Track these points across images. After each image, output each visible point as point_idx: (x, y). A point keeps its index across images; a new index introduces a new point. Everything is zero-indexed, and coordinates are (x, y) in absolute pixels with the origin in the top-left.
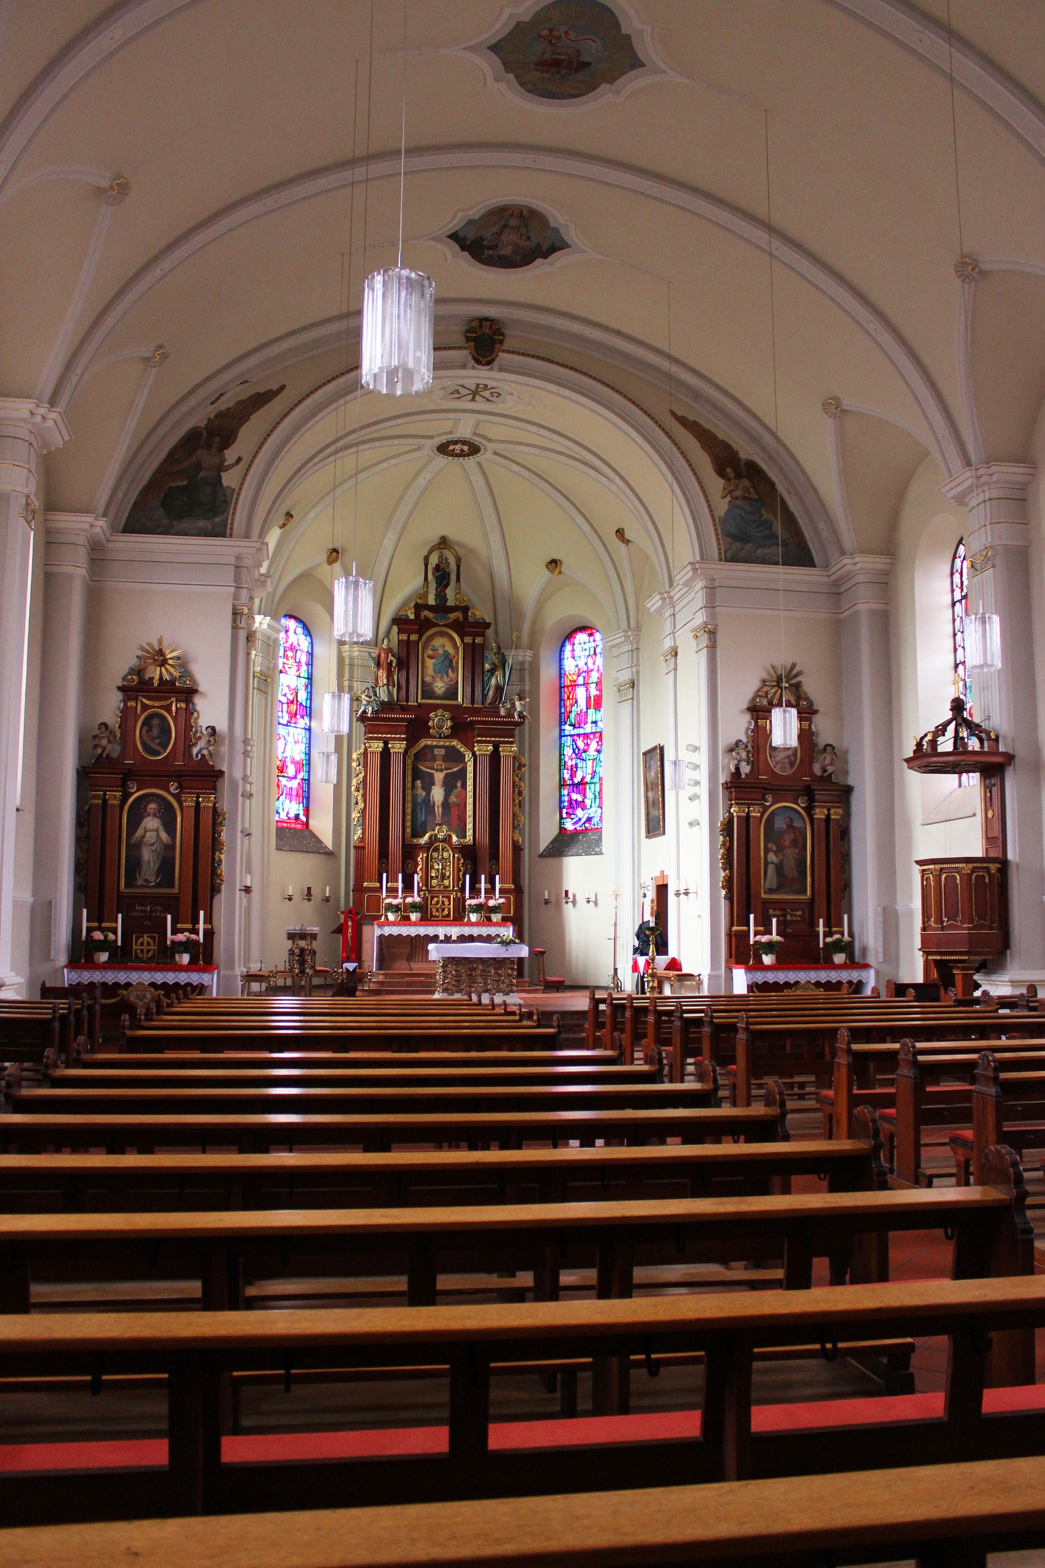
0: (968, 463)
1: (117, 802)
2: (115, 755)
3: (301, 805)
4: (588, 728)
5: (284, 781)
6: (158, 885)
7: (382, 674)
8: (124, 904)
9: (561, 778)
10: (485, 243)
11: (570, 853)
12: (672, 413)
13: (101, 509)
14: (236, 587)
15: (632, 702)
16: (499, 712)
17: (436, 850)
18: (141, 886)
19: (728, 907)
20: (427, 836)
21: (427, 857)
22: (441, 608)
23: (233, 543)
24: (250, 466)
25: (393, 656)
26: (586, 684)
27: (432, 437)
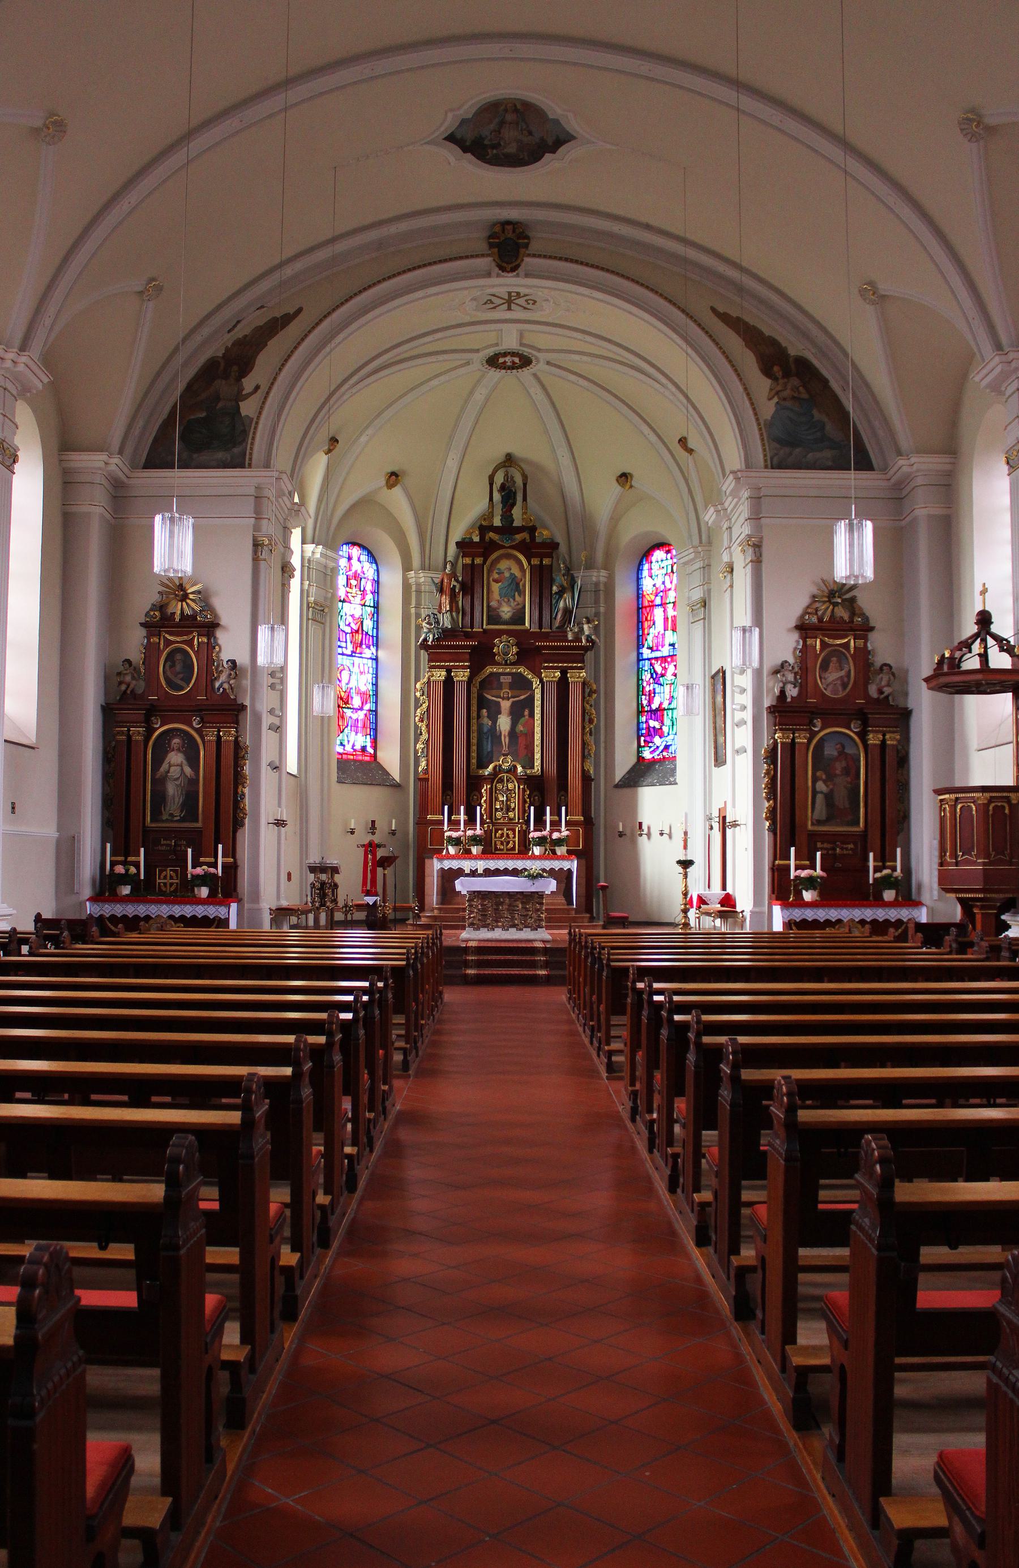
0: (998, 347)
1: (140, 738)
2: (140, 691)
3: (368, 737)
4: (665, 651)
5: (348, 713)
6: (183, 820)
7: (445, 600)
8: (150, 838)
9: (639, 704)
10: (486, 142)
11: (644, 784)
12: (713, 310)
13: (116, 443)
14: (256, 518)
15: (704, 623)
16: (567, 636)
17: (501, 781)
18: (167, 821)
19: (772, 839)
20: (491, 767)
21: (491, 789)
22: (508, 529)
23: (253, 474)
24: (268, 393)
25: (457, 581)
26: (663, 605)
27: (477, 351)
